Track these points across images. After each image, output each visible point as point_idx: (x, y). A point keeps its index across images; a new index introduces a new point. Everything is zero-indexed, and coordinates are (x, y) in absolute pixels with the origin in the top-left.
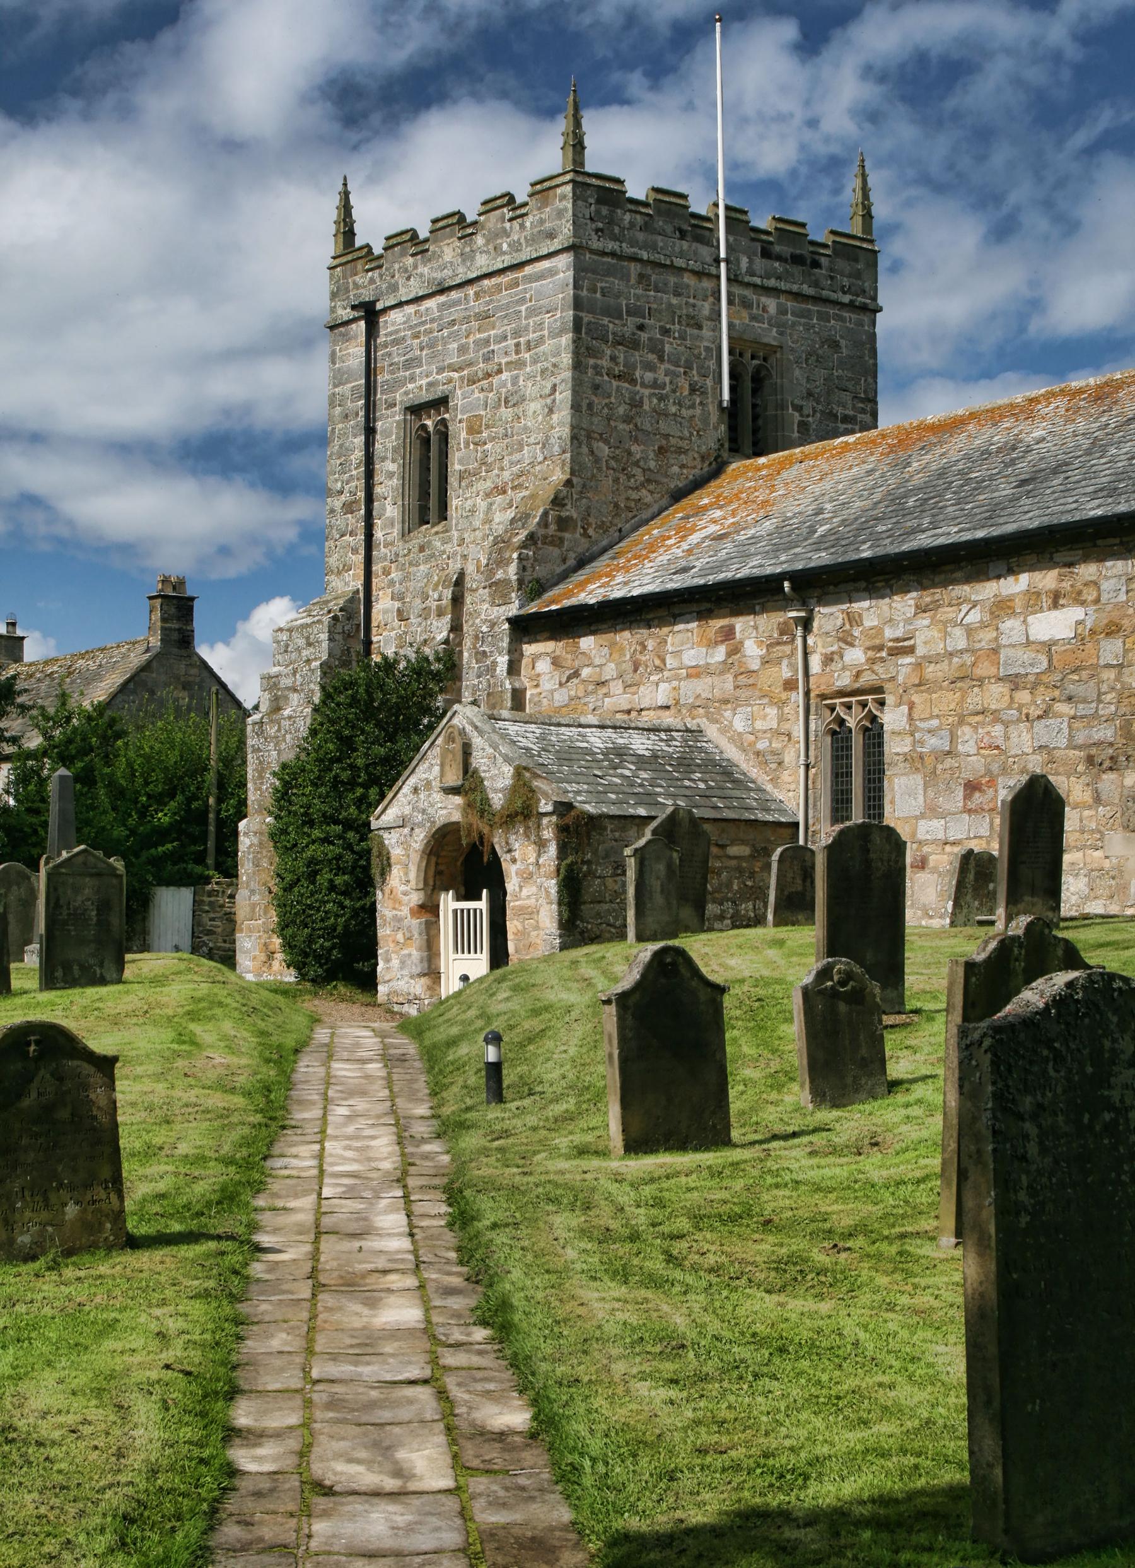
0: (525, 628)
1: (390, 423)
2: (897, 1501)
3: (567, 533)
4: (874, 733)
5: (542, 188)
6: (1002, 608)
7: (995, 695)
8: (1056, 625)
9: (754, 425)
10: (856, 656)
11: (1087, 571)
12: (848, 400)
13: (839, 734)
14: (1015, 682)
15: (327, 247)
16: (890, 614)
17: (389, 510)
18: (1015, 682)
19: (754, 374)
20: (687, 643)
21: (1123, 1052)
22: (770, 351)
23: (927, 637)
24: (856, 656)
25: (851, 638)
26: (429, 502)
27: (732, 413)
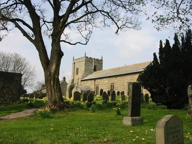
0: (81, 81)
1: (75, 69)
2: (14, 109)
3: (83, 77)
4: (113, 86)
5: (84, 57)
6: (104, 80)
7: (104, 85)
8: (106, 81)
9: (95, 70)
10: (97, 83)
11: (108, 79)
12: (101, 68)
13: (112, 86)
14: (105, 84)
15: (73, 59)
16: (99, 80)
17: (75, 74)
18: (105, 84)
19: (95, 67)
20: (89, 82)
21: (102, 102)
22: (96, 66)
23: (101, 82)
24: (97, 83)
25: (113, 80)
26: (77, 74)
27: (94, 69)
